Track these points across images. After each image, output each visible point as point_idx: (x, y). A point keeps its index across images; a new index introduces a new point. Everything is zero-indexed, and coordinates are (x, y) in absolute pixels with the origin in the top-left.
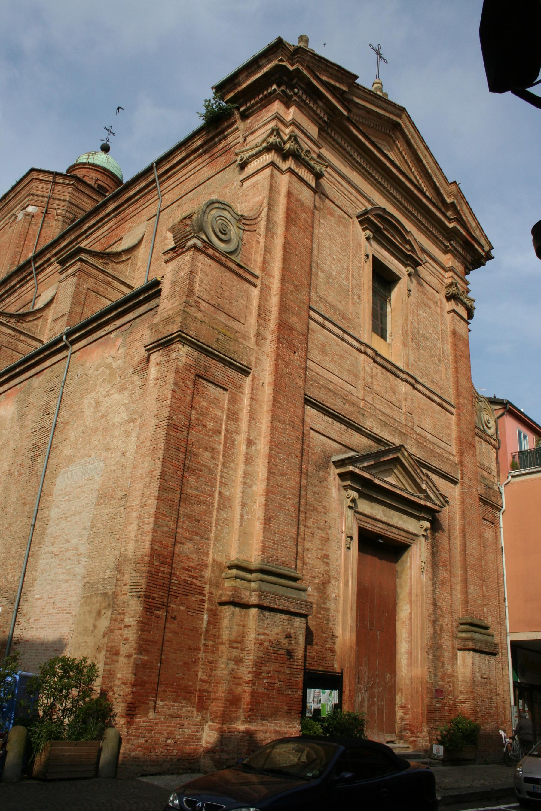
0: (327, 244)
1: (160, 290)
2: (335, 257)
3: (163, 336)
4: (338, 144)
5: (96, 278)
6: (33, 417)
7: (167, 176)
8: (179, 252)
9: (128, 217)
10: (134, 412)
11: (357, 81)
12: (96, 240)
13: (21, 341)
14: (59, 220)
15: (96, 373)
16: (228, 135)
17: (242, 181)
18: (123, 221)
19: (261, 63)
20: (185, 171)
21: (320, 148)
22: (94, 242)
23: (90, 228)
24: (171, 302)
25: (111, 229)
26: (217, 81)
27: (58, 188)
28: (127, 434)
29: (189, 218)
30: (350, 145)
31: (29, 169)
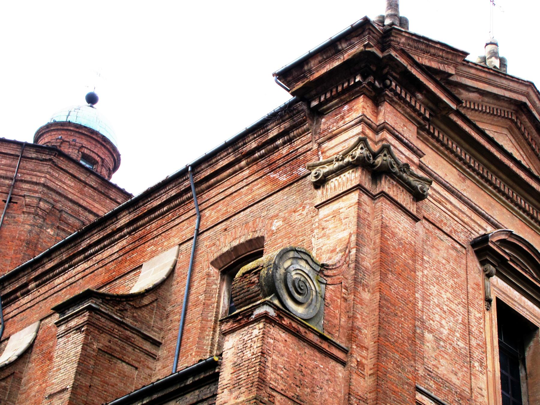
0: (434, 289)
1: (217, 375)
2: (445, 308)
4: (443, 145)
5: (111, 333)
7: (208, 184)
8: (243, 322)
11: (468, 58)
14: (29, 213)
16: (295, 137)
18: (141, 242)
19: (340, 48)
20: (233, 180)
21: (421, 157)
22: (97, 266)
23: (90, 246)
24: (235, 394)
25: (124, 251)
26: (280, 67)
27: (30, 165)
29: (256, 273)
30: (459, 144)
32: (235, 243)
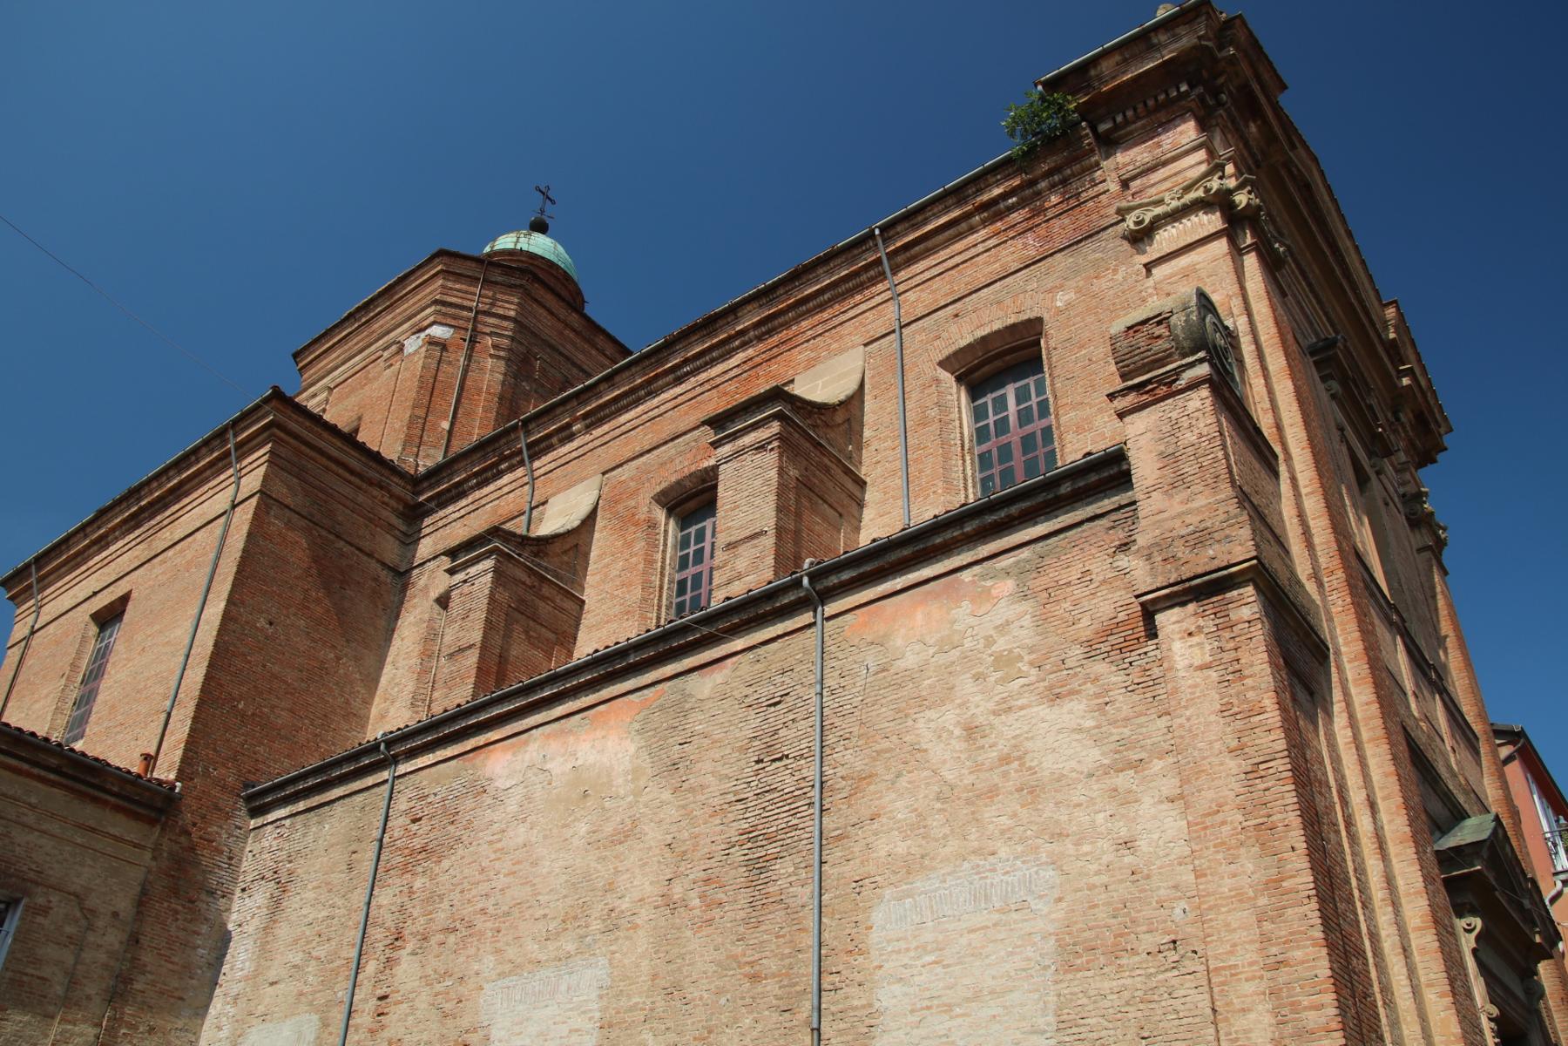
3: (1200, 570)
6: (720, 769)
9: (801, 339)
10: (1124, 744)
12: (707, 386)
13: (543, 598)
14: (498, 357)
15: (942, 659)
17: (1149, 267)
19: (1155, 41)
22: (699, 390)
23: (686, 362)
24: (1178, 498)
25: (750, 364)
28: (1125, 799)
31: (435, 250)
32: (980, 333)
